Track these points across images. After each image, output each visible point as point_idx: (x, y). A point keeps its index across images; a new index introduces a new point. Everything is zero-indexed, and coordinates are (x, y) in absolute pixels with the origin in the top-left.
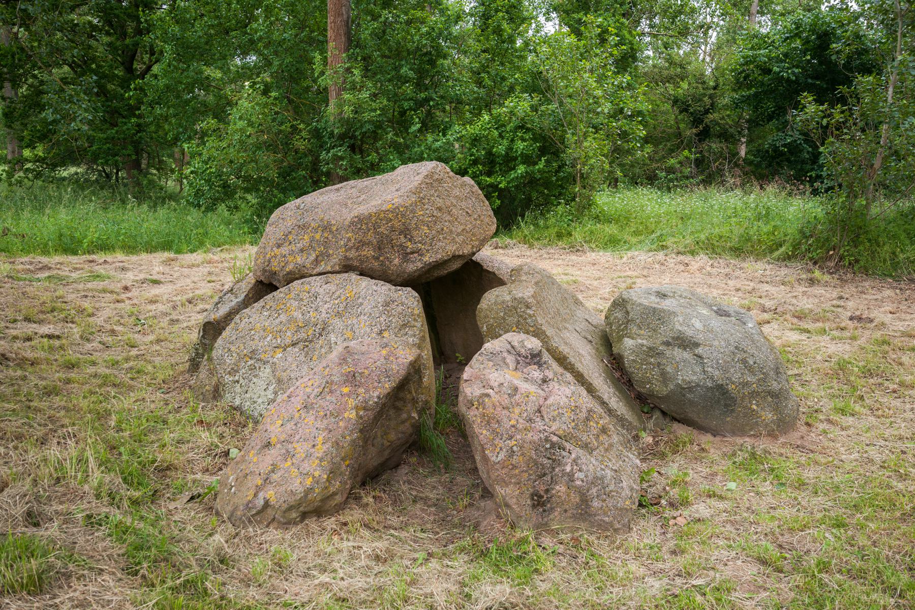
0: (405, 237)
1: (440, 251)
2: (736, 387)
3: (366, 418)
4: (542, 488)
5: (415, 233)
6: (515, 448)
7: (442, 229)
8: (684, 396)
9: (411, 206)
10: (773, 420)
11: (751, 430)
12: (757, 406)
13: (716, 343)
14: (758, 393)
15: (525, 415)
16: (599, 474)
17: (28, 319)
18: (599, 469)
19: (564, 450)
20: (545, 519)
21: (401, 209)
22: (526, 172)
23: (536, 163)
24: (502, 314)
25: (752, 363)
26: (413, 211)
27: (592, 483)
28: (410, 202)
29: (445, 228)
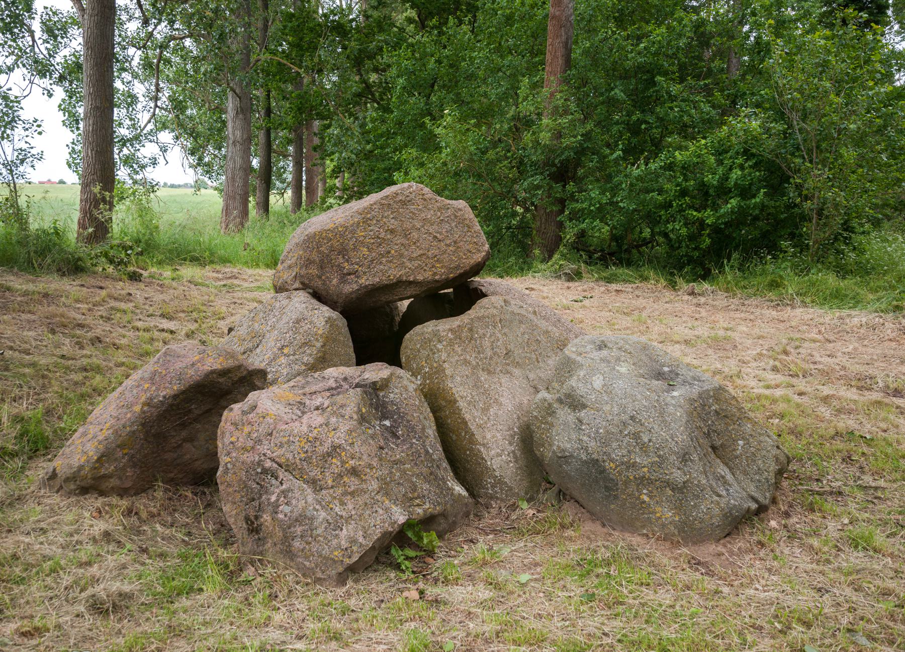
0: (344, 258)
1: (381, 274)
2: (617, 466)
3: (149, 414)
4: (252, 514)
5: (352, 254)
6: (229, 466)
7: (389, 252)
8: (561, 466)
9: (352, 226)
10: (674, 521)
11: (643, 527)
12: (651, 497)
13: (607, 408)
14: (651, 482)
15: (255, 435)
16: (308, 514)
17: (163, 316)
18: (311, 508)
19: (276, 478)
20: (261, 548)
21: (340, 229)
22: (740, 207)
23: (754, 196)
24: (418, 346)
25: (646, 440)
26: (353, 232)
27: (296, 520)
28: (351, 222)
29: (393, 252)
